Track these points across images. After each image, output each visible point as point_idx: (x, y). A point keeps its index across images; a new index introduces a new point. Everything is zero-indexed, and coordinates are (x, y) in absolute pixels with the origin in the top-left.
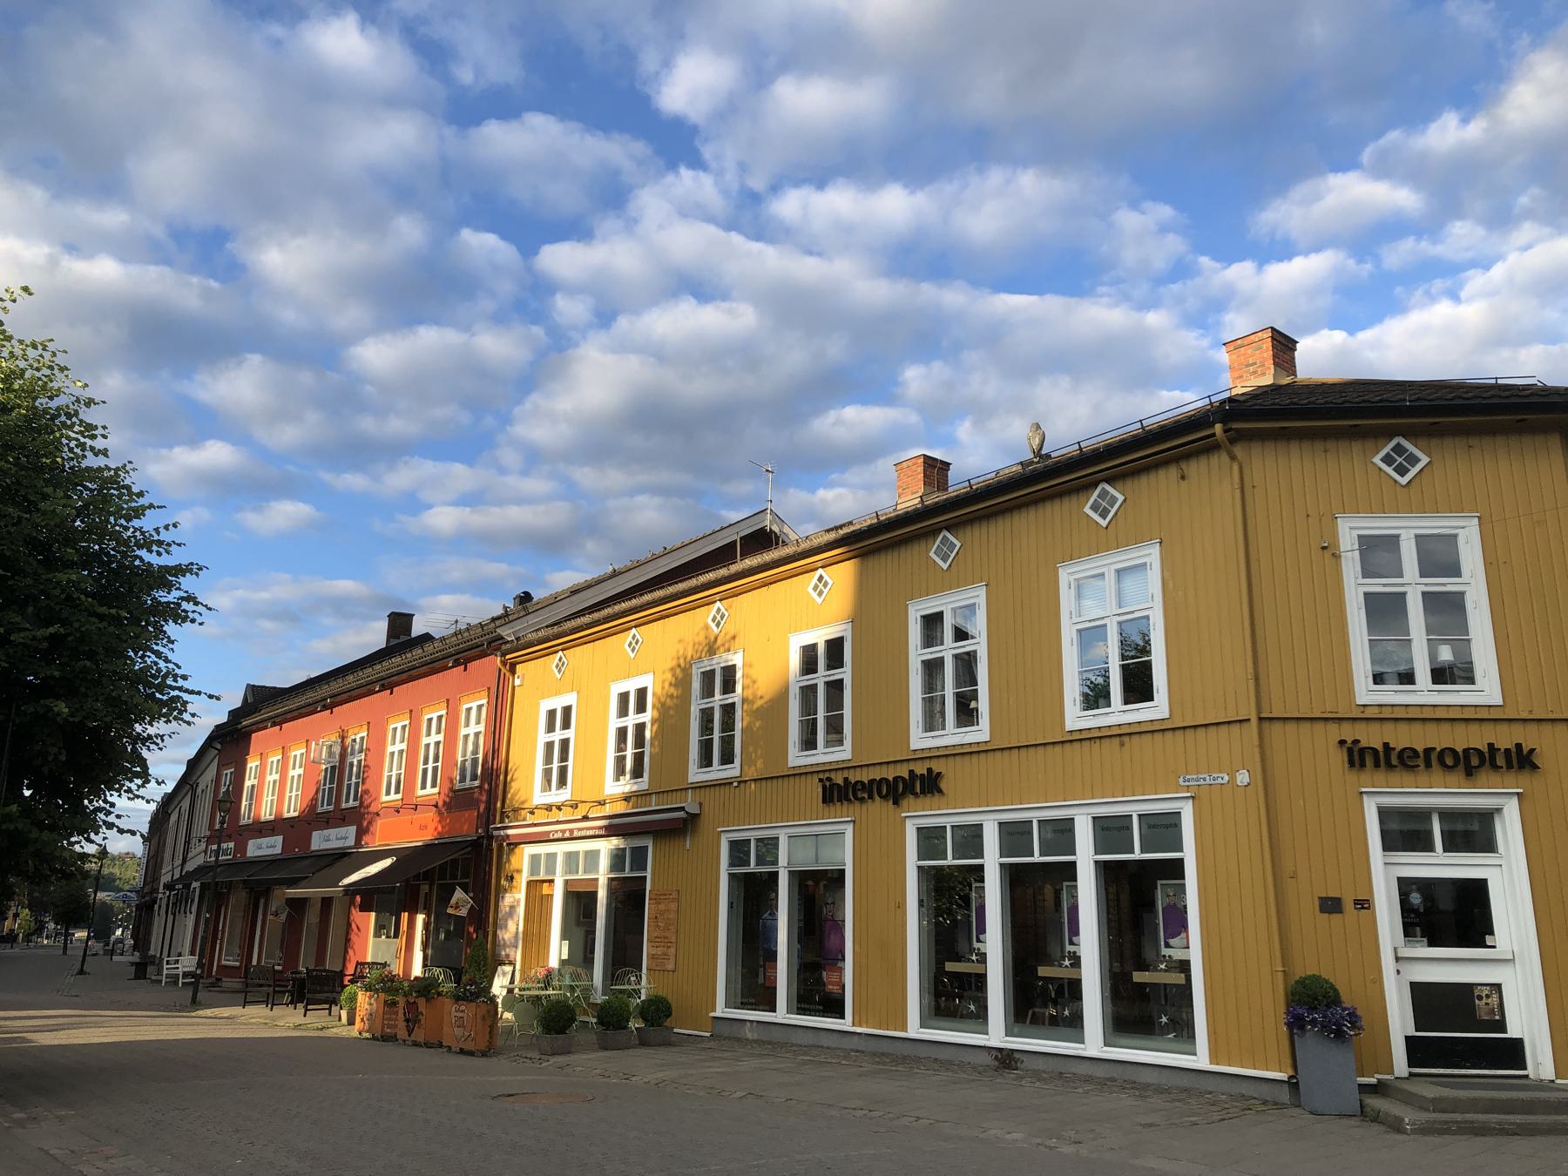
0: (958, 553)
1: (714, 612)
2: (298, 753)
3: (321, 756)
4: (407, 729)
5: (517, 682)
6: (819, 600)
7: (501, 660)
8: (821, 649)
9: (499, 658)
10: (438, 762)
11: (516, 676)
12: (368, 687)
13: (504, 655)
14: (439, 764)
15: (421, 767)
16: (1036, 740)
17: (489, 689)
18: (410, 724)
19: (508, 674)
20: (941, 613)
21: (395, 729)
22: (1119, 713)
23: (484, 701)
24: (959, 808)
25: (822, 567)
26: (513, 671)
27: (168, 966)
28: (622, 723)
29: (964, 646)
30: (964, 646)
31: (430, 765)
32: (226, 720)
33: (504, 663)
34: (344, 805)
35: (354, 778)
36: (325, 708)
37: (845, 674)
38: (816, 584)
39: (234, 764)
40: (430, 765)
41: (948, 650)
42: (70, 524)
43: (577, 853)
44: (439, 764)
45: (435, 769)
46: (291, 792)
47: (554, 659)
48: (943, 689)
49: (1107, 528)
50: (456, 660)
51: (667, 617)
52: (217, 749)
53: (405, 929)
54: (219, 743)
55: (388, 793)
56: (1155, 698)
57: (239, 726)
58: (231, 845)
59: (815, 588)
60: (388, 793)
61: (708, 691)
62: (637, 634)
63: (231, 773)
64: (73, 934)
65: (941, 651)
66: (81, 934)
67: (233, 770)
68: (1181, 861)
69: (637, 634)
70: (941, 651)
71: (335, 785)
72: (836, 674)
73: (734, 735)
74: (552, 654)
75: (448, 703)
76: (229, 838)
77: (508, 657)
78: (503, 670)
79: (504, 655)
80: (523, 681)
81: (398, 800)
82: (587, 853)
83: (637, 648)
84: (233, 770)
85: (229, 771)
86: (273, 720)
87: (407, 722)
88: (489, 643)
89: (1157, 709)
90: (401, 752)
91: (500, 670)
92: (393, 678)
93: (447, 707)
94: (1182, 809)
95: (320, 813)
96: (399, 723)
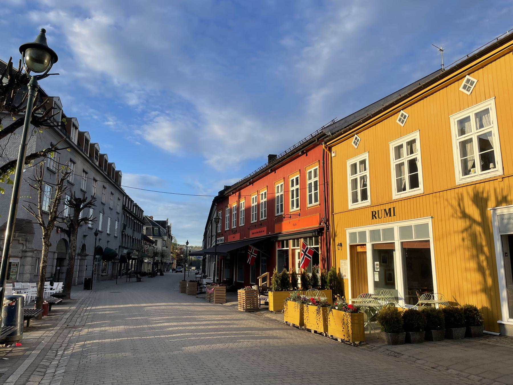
0: (475, 86)
1: (399, 116)
2: (254, 197)
3: (116, 260)
4: (283, 186)
5: (333, 155)
6: (402, 125)
7: (324, 146)
8: (254, 206)
9: (323, 145)
10: (309, 195)
11: (332, 152)
12: (266, 171)
13: (326, 143)
14: (299, 197)
15: (291, 200)
16: (437, 191)
17: (319, 161)
18: (284, 183)
19: (328, 152)
20: (469, 117)
21: (278, 187)
22: (409, 192)
23: (317, 167)
24: (410, 219)
25: (402, 110)
26: (330, 149)
27: (209, 276)
28: (354, 177)
29: (484, 130)
30: (484, 130)
31: (295, 199)
32: (218, 195)
33: (326, 147)
34: (261, 219)
35: (242, 216)
36: (250, 184)
37: (418, 155)
38: (355, 141)
39: (221, 210)
40: (295, 199)
41: (406, 158)
42: (131, 255)
43: (379, 231)
44: (299, 197)
45: (297, 200)
46: (293, 197)
47: (462, 82)
48: (473, 153)
49: (403, 127)
50: (271, 170)
51: (426, 97)
52: (216, 205)
53: (291, 267)
54: (216, 203)
55: (311, 202)
56: (368, 199)
57: (224, 194)
58: (223, 238)
59: (354, 142)
60: (311, 202)
61: (398, 155)
62: (357, 137)
63: (221, 213)
64: (191, 268)
65: (356, 176)
66: (194, 268)
67: (221, 212)
68: (295, 247)
69: (357, 137)
70: (356, 176)
71: (266, 209)
72: (364, 173)
73: (493, 151)
74: (394, 114)
75: (245, 198)
76: (222, 235)
77: (327, 144)
78: (326, 150)
79: (326, 143)
80: (336, 154)
81: (318, 205)
82: (360, 233)
83: (405, 120)
84: (221, 212)
85: (220, 212)
86: (232, 192)
87: (283, 183)
88: (318, 139)
89: (419, 190)
90: (236, 213)
91: (324, 150)
92: (276, 166)
93: (319, 164)
94: (429, 222)
95: (240, 227)
96: (280, 184)
